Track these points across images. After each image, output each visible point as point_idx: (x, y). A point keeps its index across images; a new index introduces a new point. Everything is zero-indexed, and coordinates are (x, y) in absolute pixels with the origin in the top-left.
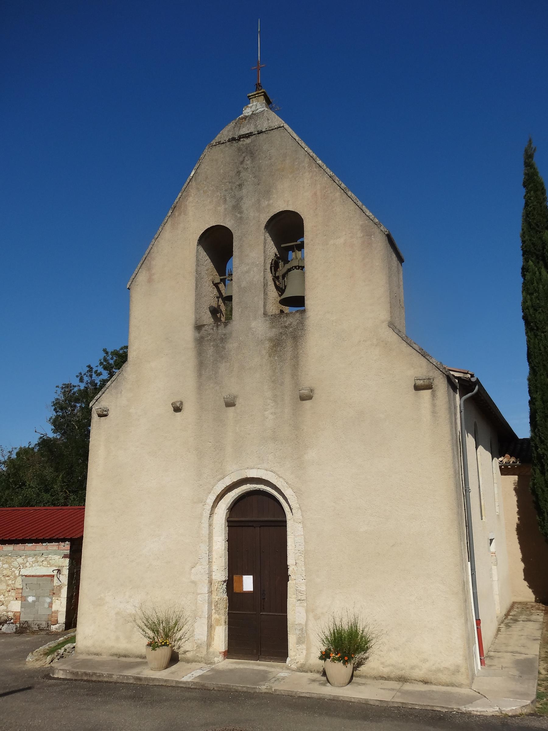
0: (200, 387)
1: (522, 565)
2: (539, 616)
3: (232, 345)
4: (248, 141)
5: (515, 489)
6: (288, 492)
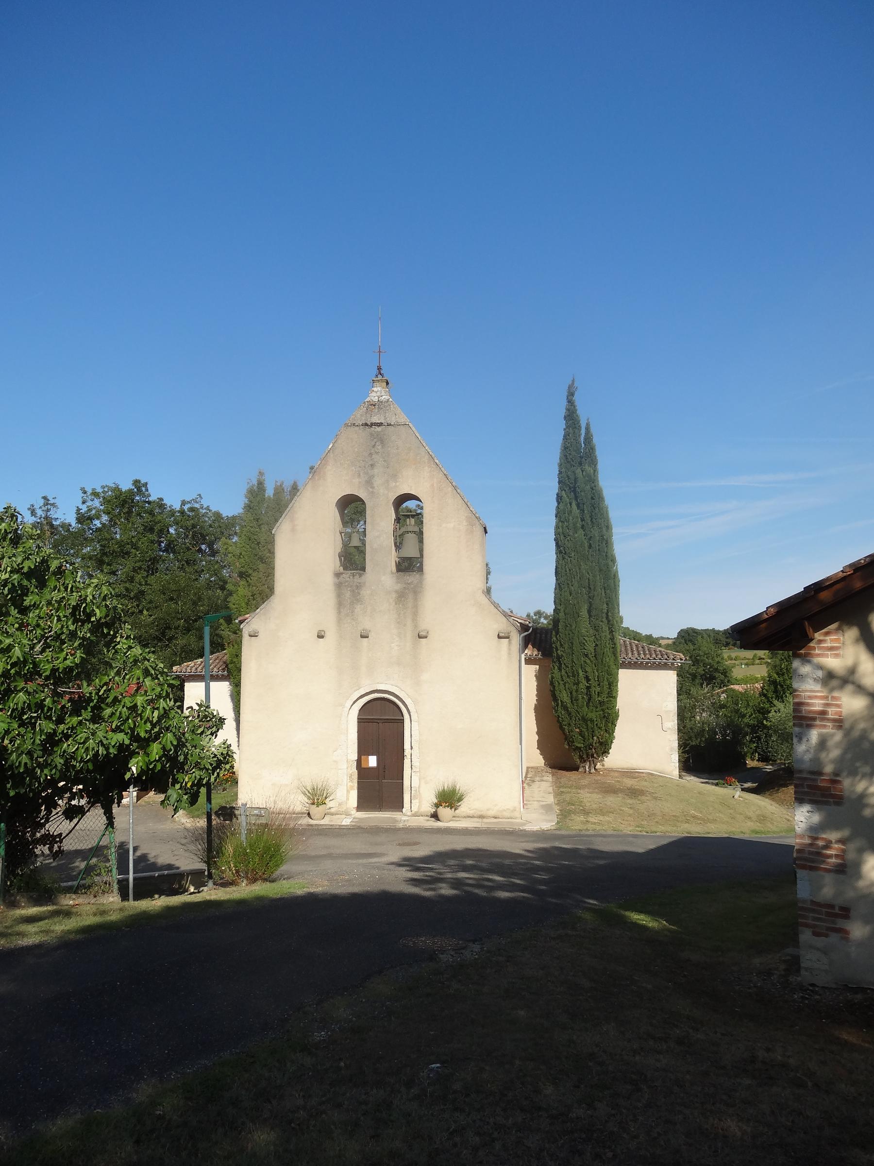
0: (339, 621)
1: (537, 737)
2: (549, 778)
3: (365, 592)
4: (379, 429)
5: (536, 676)
6: (408, 701)
